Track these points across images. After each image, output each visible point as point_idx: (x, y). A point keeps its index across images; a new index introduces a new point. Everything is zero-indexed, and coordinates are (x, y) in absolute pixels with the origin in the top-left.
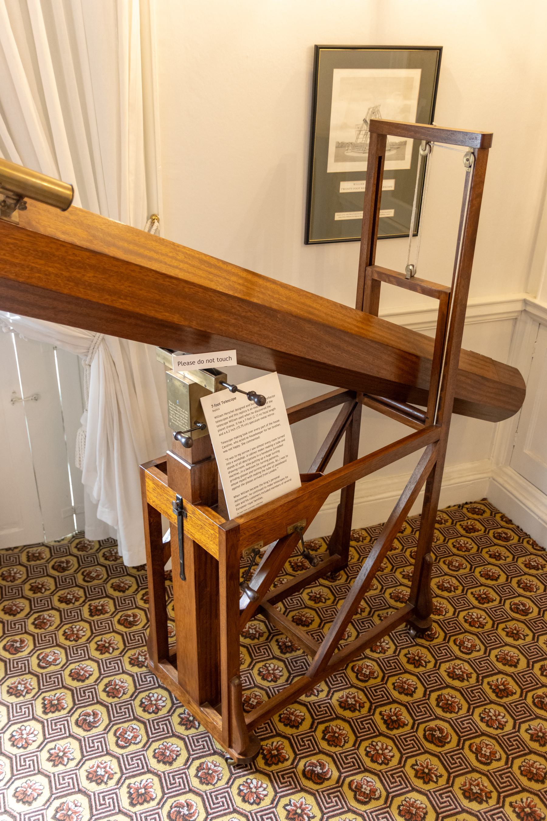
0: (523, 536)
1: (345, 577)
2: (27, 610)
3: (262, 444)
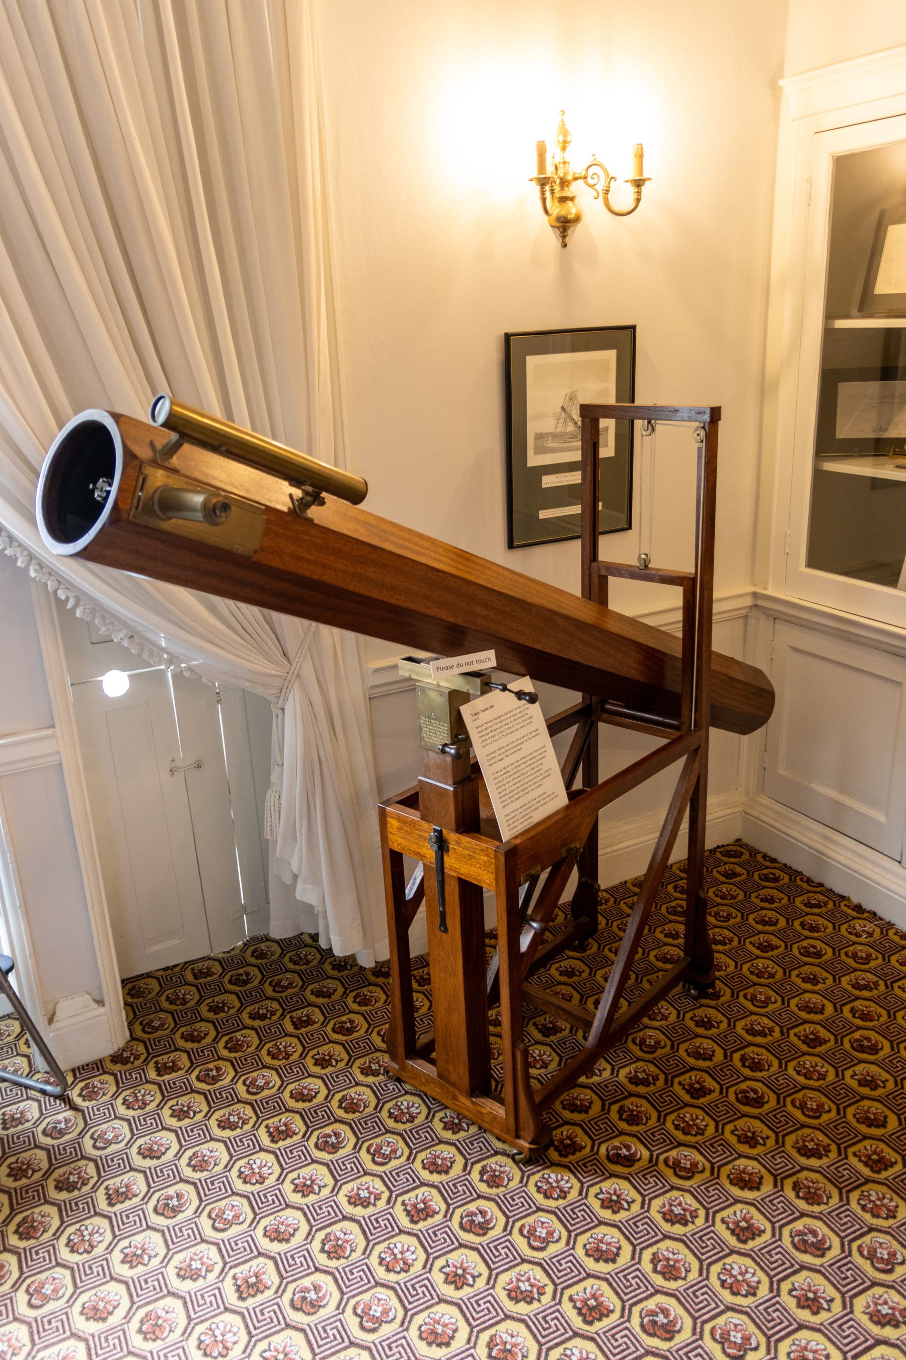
0: (795, 874)
1: (595, 946)
2: (304, 1228)
3: (522, 759)
